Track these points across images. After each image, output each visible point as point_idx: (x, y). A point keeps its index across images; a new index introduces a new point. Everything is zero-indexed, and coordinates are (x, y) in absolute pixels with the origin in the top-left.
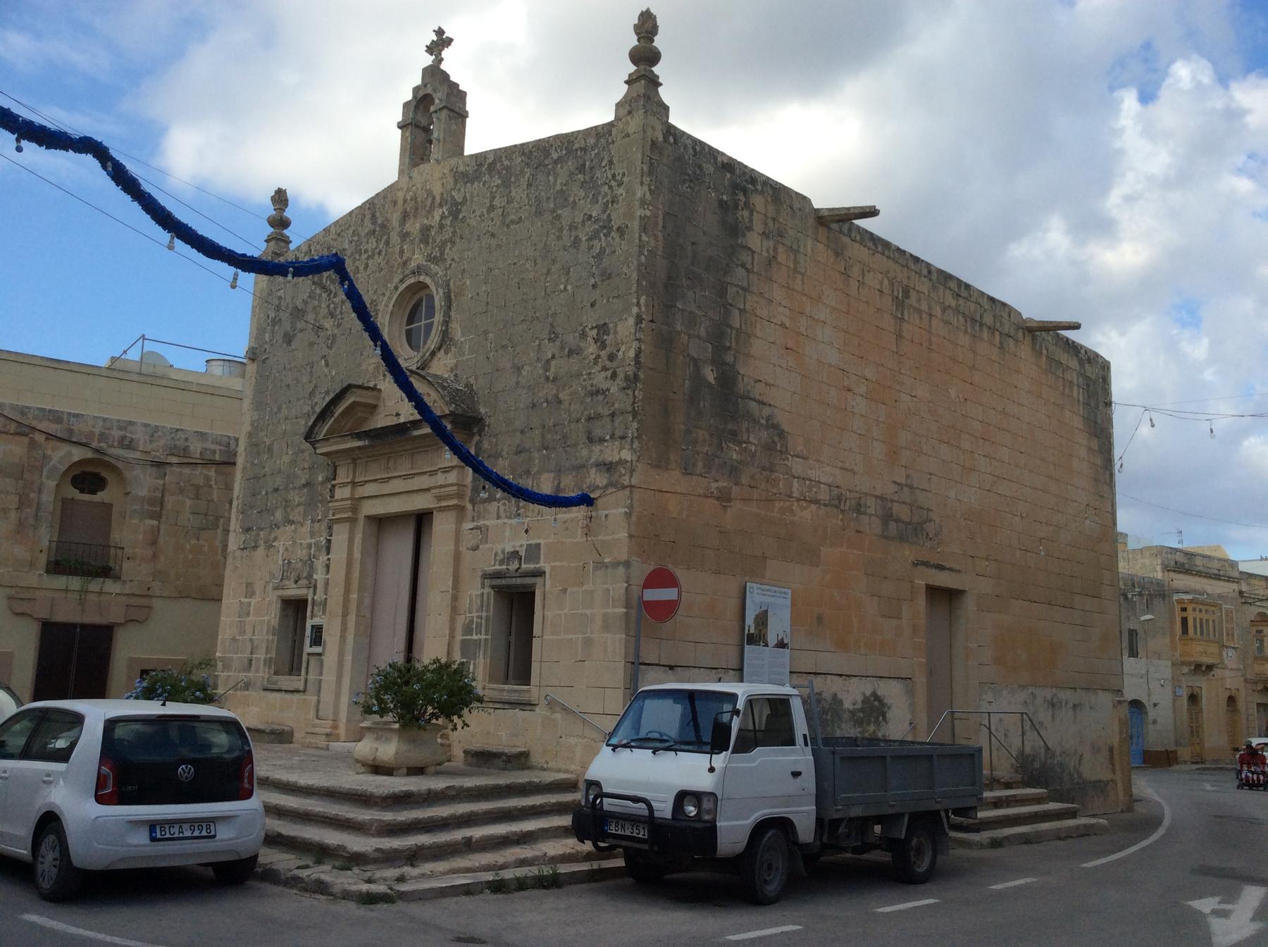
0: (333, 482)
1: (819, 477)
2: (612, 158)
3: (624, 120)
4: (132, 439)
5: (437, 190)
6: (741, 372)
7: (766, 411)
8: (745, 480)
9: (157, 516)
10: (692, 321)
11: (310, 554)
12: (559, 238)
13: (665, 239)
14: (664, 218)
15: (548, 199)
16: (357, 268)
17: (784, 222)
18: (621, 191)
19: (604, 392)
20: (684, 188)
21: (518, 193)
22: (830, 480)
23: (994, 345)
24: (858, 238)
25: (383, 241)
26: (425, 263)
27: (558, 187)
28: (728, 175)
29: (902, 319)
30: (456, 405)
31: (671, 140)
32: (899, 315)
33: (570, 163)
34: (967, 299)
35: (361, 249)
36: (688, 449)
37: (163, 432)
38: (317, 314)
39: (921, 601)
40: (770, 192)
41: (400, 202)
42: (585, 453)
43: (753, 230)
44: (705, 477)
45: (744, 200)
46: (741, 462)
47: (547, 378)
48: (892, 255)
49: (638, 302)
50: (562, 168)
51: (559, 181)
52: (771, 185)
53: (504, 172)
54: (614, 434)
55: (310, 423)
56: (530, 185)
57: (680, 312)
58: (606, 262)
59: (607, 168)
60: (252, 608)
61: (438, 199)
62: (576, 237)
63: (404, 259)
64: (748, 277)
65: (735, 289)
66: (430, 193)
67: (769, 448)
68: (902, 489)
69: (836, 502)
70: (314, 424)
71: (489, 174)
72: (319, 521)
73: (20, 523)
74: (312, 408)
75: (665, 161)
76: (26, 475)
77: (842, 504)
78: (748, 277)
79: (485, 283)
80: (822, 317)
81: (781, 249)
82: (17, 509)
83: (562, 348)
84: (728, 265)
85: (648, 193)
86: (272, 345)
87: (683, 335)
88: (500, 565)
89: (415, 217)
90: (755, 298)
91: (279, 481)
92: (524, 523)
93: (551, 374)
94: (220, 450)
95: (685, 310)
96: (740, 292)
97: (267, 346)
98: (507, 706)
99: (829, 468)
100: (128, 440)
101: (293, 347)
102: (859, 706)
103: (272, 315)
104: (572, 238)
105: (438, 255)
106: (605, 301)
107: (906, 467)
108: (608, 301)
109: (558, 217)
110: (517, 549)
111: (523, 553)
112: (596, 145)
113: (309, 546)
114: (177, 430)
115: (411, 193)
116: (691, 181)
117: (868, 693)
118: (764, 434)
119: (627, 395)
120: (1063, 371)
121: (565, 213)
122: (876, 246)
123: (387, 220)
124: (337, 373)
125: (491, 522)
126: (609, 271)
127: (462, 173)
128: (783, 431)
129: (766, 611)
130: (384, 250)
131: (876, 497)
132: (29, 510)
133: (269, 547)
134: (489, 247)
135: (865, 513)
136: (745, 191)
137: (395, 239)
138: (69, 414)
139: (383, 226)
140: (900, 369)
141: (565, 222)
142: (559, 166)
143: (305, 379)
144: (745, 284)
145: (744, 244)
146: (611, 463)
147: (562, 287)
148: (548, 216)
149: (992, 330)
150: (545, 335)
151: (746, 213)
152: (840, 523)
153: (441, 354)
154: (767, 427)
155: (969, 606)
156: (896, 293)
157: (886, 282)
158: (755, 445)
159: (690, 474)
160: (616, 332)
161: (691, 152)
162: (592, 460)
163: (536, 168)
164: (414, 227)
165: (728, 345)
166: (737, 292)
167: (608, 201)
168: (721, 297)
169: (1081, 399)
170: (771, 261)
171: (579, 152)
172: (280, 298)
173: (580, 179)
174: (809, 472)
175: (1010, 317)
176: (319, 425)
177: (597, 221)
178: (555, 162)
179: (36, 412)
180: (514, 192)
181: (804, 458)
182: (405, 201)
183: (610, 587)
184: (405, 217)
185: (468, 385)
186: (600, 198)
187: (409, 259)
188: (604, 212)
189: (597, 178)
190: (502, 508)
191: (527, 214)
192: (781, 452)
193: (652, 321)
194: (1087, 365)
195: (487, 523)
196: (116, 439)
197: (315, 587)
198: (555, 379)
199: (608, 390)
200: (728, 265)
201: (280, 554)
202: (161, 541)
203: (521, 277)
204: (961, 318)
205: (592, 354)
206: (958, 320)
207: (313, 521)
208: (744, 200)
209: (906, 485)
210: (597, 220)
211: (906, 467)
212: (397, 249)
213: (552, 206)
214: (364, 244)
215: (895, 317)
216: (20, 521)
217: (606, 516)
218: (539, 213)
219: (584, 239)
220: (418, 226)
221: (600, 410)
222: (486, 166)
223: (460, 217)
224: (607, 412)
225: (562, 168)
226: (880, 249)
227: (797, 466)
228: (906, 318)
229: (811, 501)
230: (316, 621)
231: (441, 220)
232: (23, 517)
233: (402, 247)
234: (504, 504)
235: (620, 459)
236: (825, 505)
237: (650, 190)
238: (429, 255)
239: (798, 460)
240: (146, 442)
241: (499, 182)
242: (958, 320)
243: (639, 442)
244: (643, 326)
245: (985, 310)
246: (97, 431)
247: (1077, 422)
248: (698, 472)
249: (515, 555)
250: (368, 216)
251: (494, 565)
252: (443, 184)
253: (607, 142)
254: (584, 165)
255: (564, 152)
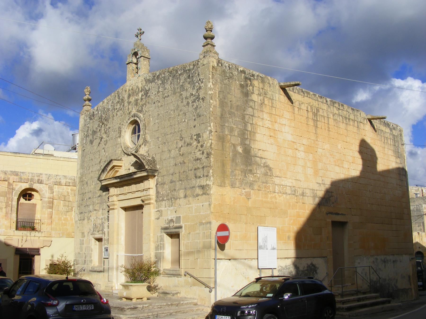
0: (109, 195)
1: (286, 184)
2: (199, 73)
3: (202, 59)
4: (42, 180)
5: (140, 86)
6: (252, 147)
7: (264, 161)
8: (256, 187)
9: (52, 208)
10: (231, 130)
11: (102, 221)
12: (182, 102)
13: (219, 101)
14: (219, 93)
15: (178, 88)
16: (114, 115)
17: (267, 89)
18: (202, 85)
19: (200, 159)
20: (226, 81)
21: (167, 86)
22: (291, 185)
23: (355, 126)
24: (297, 92)
25: (122, 105)
26: (136, 113)
27: (181, 84)
28: (243, 75)
29: (317, 120)
30: (148, 166)
31: (220, 65)
32: (316, 119)
33: (185, 75)
34: (343, 110)
35: (115, 108)
36: (232, 178)
37: (52, 177)
38: (101, 133)
39: (330, 227)
40: (260, 78)
41: (128, 91)
42: (194, 182)
43: (254, 93)
44: (240, 188)
45: (250, 83)
46: (254, 181)
47: (180, 154)
48: (311, 97)
49: (210, 125)
50: (182, 77)
51: (181, 82)
52: (260, 76)
53: (162, 79)
54: (204, 175)
55: (100, 173)
56: (171, 83)
57: (227, 127)
58: (198, 111)
59: (197, 77)
60: (84, 242)
61: (140, 89)
62: (188, 102)
63: (129, 111)
64: (253, 111)
65: (248, 116)
66: (137, 87)
67: (266, 174)
68: (320, 185)
69: (294, 193)
70: (101, 174)
71: (157, 80)
72: (105, 209)
73: (7, 213)
74: (100, 168)
75: (218, 73)
76: (8, 196)
77: (296, 193)
78: (253, 111)
79: (157, 119)
80: (284, 123)
81: (266, 99)
82: (5, 208)
83: (185, 143)
84: (245, 107)
85: (212, 85)
86: (86, 144)
87: (228, 136)
88: (167, 224)
89: (133, 96)
90: (257, 119)
91: (90, 195)
92: (174, 209)
93: (181, 153)
94: (72, 182)
95: (229, 126)
96: (250, 117)
97: (85, 145)
98: (172, 276)
99: (290, 180)
100: (40, 180)
101: (93, 145)
102: (306, 268)
103: (86, 133)
104: (187, 102)
105: (141, 109)
106: (199, 125)
107: (321, 177)
108: (200, 125)
109: (181, 95)
110: (173, 218)
111: (174, 220)
112: (193, 68)
113: (102, 219)
114: (57, 175)
115: (131, 87)
116: (229, 79)
117: (309, 264)
118: (263, 170)
119: (208, 160)
120: (384, 134)
121: (184, 94)
122: (304, 93)
123: (123, 97)
124: (108, 154)
125: (163, 209)
126: (200, 114)
127: (148, 79)
128: (271, 168)
129: (266, 237)
130: (122, 108)
131: (310, 189)
132: (9, 208)
133: (89, 219)
134: (158, 106)
135: (306, 196)
136: (250, 80)
137: (126, 104)
138: (20, 172)
139: (122, 100)
140: (317, 139)
141: (184, 96)
142: (181, 76)
143: (97, 157)
144: (252, 114)
145: (251, 99)
146: (203, 186)
147: (184, 120)
148: (178, 95)
149: (354, 121)
150: (178, 138)
151: (251, 88)
152: (296, 201)
153: (143, 146)
154: (264, 167)
155: (349, 227)
156: (313, 111)
157: (309, 107)
158: (259, 174)
159: (234, 187)
160: (203, 137)
161: (228, 68)
162: (197, 185)
163: (173, 77)
164: (132, 99)
165: (246, 137)
166: (249, 117)
167: (198, 88)
168: (243, 120)
169: (392, 144)
170: (262, 104)
171: (188, 71)
172: (88, 127)
173: (188, 81)
174: (282, 182)
175: (360, 115)
176: (102, 175)
177: (195, 96)
178: (180, 75)
179: (10, 172)
180: (166, 86)
181: (279, 177)
182: (129, 90)
183: (205, 232)
184: (129, 96)
185: (153, 158)
186: (195, 87)
187: (131, 112)
188: (197, 92)
189: (194, 80)
190: (167, 203)
191: (170, 94)
192: (270, 176)
193: (216, 132)
194: (393, 131)
195: (162, 209)
196: (36, 180)
197: (105, 233)
198: (183, 155)
199: (201, 158)
200: (245, 107)
201: (92, 222)
202: (53, 216)
203: (169, 117)
204: (340, 117)
205: (195, 145)
206: (339, 118)
207: (102, 210)
208: (250, 83)
209: (322, 184)
210: (195, 95)
211: (321, 177)
212: (127, 108)
213: (179, 90)
214: (116, 106)
215: (314, 120)
216: (6, 212)
217: (203, 205)
218: (175, 93)
219: (190, 102)
220: (134, 99)
221: (199, 166)
222: (156, 77)
223: (148, 95)
224: (201, 167)
225: (182, 77)
226: (306, 95)
227: (277, 181)
228: (318, 120)
229: (284, 194)
230: (106, 246)
231: (141, 97)
232: (7, 210)
233: (129, 107)
234: (167, 202)
235: (206, 184)
236: (289, 194)
237: (213, 84)
238: (138, 110)
239: (277, 178)
240: (46, 181)
241: (161, 82)
242: (339, 118)
243: (213, 178)
244: (212, 134)
245: (350, 114)
246: (30, 178)
247: (391, 153)
248: (237, 186)
249: (172, 220)
250: (117, 96)
251: (165, 225)
252: (142, 84)
253: (197, 67)
254: (189, 76)
255: (183, 71)
